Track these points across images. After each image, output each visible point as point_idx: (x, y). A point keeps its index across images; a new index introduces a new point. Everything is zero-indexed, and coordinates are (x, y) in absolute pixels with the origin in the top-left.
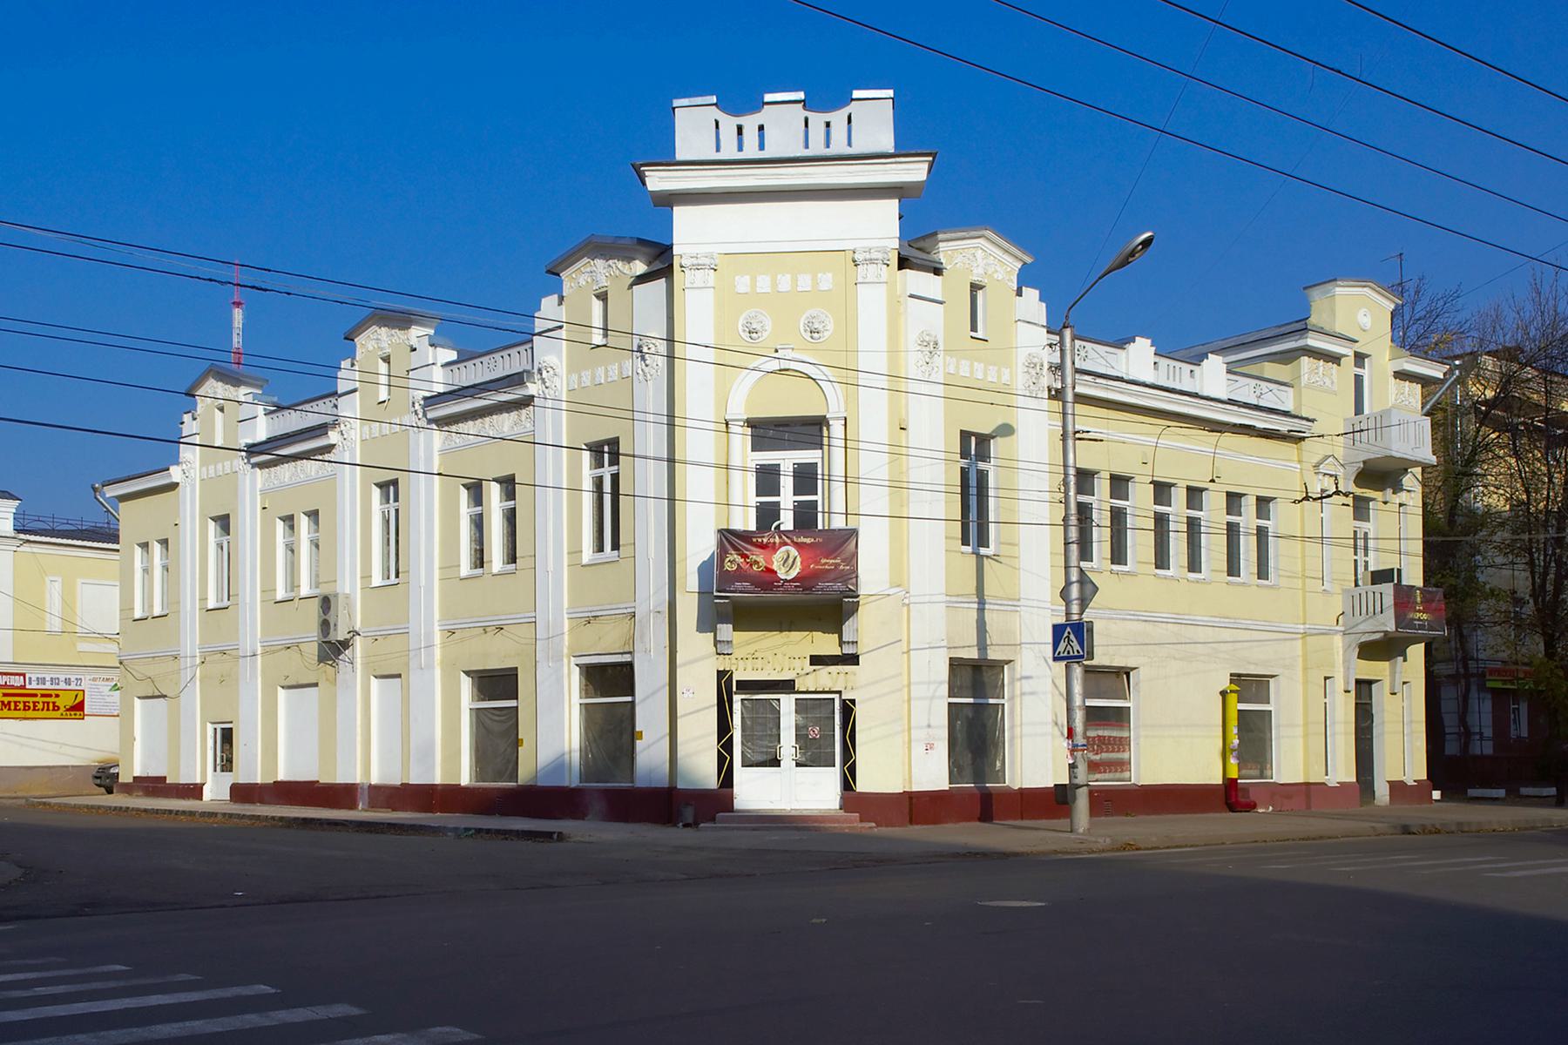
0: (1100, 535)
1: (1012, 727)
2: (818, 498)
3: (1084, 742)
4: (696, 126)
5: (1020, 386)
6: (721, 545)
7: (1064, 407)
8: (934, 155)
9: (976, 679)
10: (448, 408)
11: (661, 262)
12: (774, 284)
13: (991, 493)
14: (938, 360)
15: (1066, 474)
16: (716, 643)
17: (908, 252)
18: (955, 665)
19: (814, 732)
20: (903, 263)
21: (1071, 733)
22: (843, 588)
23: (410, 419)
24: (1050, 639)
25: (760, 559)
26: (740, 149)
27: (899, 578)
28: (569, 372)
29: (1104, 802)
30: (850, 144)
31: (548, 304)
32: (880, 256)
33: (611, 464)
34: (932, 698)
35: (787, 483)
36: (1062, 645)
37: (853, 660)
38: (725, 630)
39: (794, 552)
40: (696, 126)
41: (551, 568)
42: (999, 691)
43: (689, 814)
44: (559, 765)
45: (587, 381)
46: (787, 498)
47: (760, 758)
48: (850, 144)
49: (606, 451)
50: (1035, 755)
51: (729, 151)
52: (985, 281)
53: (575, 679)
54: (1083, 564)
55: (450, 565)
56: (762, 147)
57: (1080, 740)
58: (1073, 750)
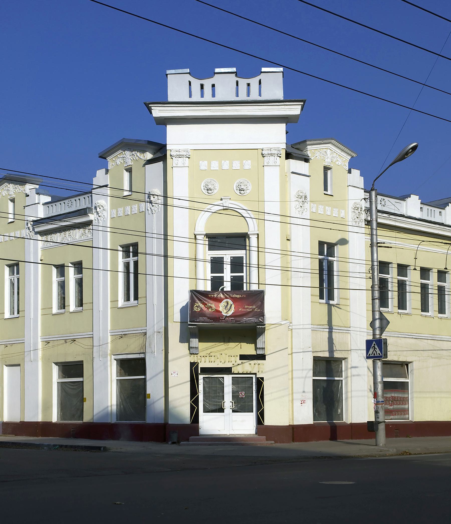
0: (392, 295)
1: (347, 392)
2: (244, 274)
3: (382, 400)
4: (178, 84)
5: (350, 219)
6: (192, 298)
7: (372, 232)
8: (304, 101)
9: (328, 369)
10: (46, 227)
11: (160, 153)
12: (220, 165)
13: (335, 273)
14: (307, 206)
15: (373, 265)
16: (190, 348)
17: (291, 150)
18: (316, 360)
19: (242, 394)
20: (288, 156)
21: (375, 395)
22: (256, 320)
23: (25, 233)
24: (365, 348)
25: (213, 306)
26: (202, 96)
27: (286, 315)
28: (112, 208)
29: (394, 430)
30: (260, 95)
31: (100, 173)
32: (276, 152)
33: (133, 256)
34: (306, 377)
35: (227, 268)
36: (371, 351)
37: (262, 357)
38: (195, 342)
39: (230, 302)
40: (178, 84)
41: (101, 309)
42: (340, 374)
43: (175, 437)
44: (108, 414)
45: (121, 213)
46: (227, 274)
47: (213, 408)
48: (260, 95)
49: (132, 250)
50: (358, 406)
51: (196, 97)
52: (332, 165)
53: (113, 368)
54: (381, 309)
55: (47, 307)
56: (213, 95)
57: (380, 399)
58: (377, 403)
